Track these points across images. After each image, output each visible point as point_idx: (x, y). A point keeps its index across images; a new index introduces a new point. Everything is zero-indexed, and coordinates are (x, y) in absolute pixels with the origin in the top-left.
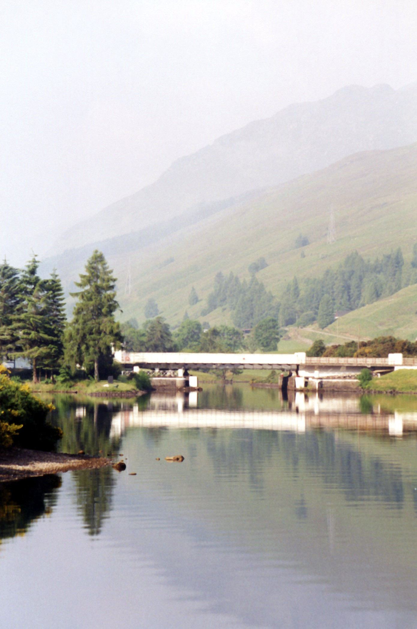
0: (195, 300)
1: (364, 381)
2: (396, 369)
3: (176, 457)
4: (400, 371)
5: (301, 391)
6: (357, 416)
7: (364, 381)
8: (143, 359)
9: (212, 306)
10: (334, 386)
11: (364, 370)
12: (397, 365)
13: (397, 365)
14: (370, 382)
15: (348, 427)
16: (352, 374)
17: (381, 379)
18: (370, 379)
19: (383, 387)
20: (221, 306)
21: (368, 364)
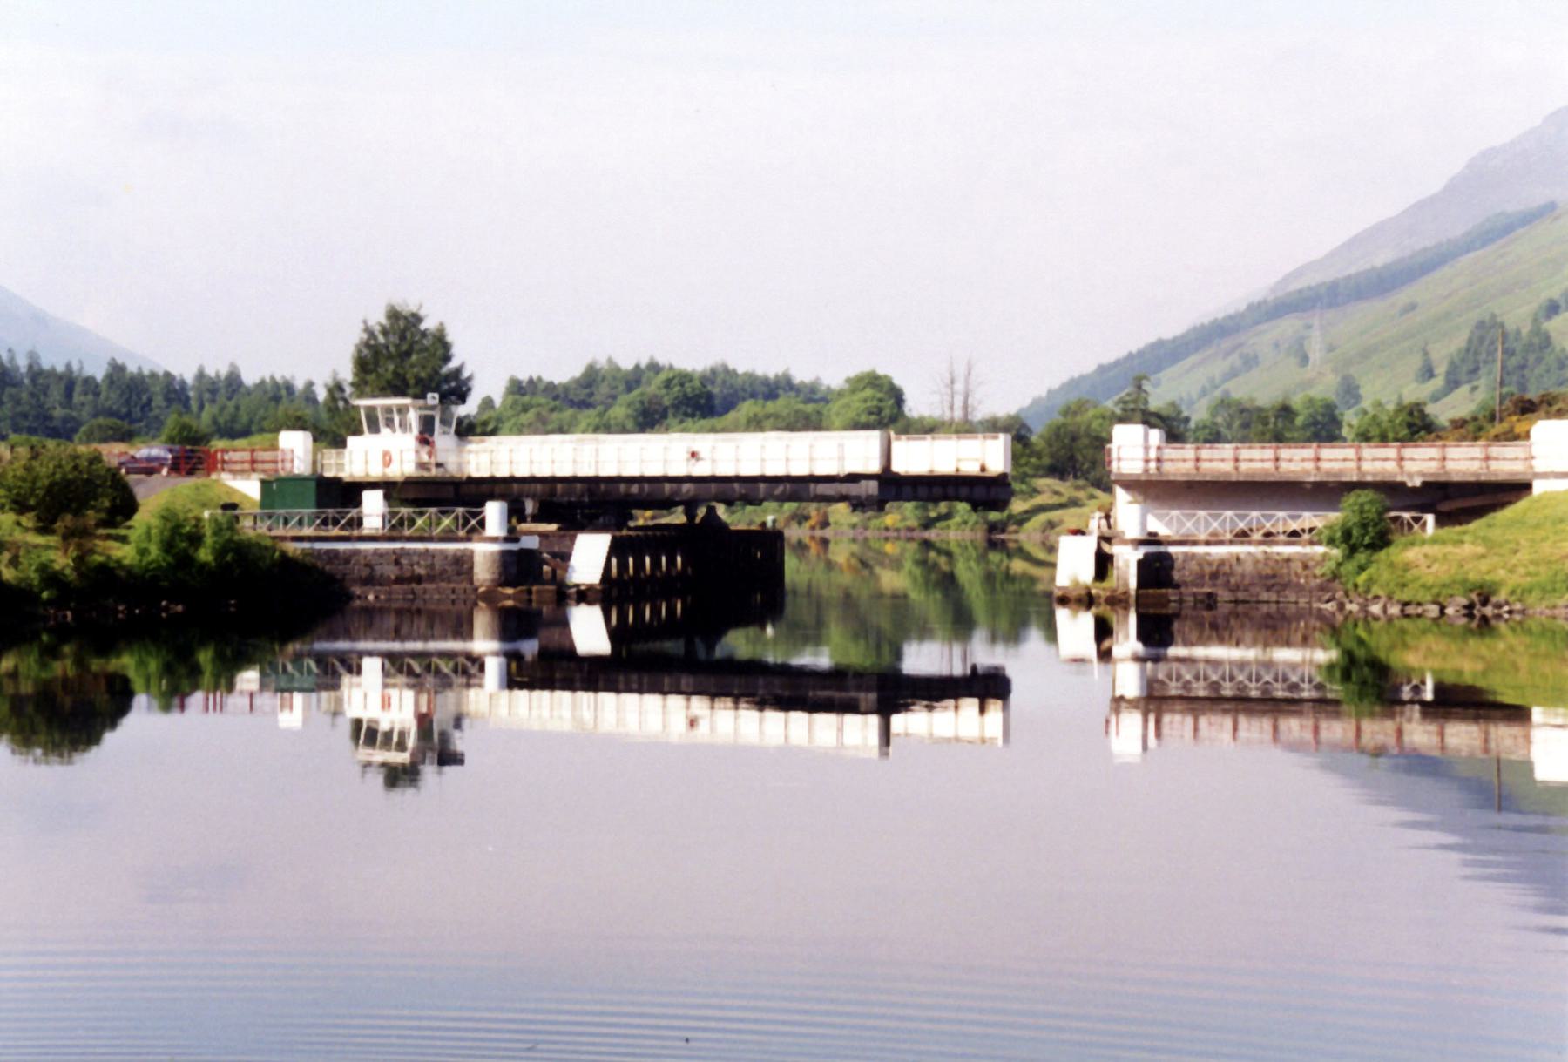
0: (1428, 373)
1: (1353, 550)
2: (1539, 487)
3: (466, 723)
4: (1549, 497)
5: (1087, 600)
6: (1237, 711)
7: (1353, 550)
8: (563, 442)
9: (1453, 384)
10: (1214, 576)
11: (1351, 499)
12: (1545, 476)
13: (1545, 476)
14: (1382, 554)
15: (265, 392)
16: (1308, 519)
17: (1434, 541)
18: (1381, 541)
19: (1430, 580)
20: (1469, 381)
21: (1411, 475)
